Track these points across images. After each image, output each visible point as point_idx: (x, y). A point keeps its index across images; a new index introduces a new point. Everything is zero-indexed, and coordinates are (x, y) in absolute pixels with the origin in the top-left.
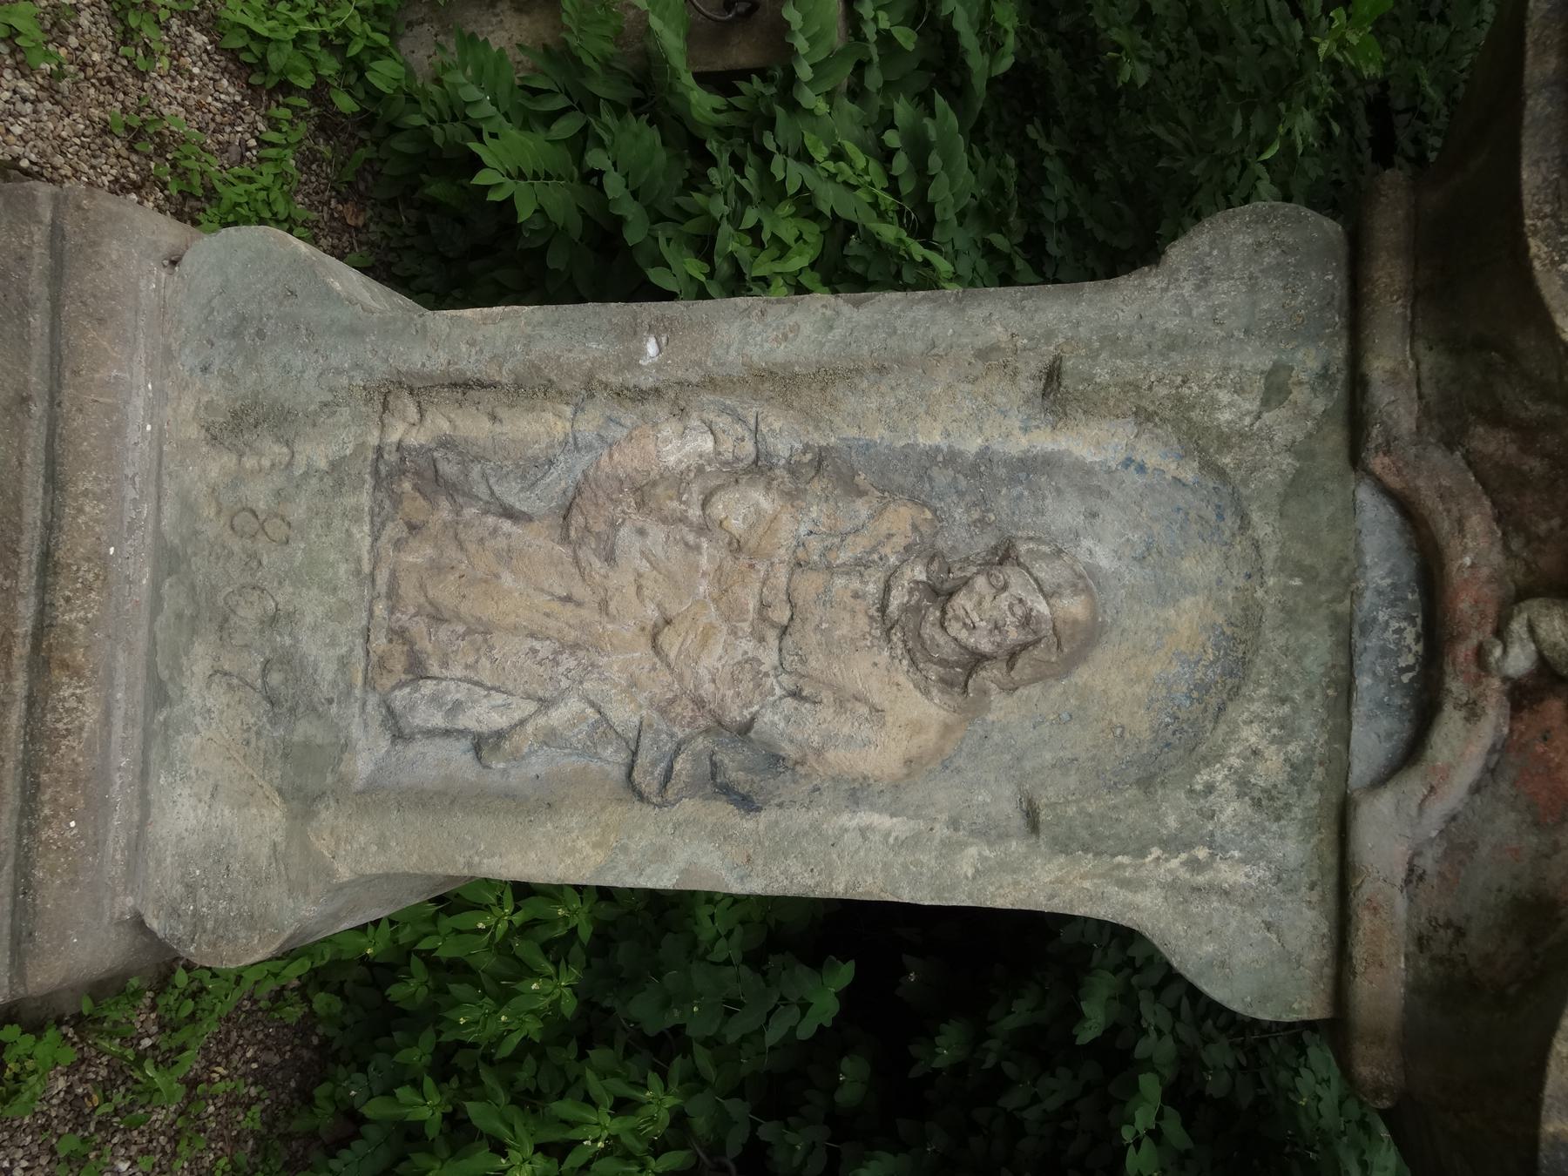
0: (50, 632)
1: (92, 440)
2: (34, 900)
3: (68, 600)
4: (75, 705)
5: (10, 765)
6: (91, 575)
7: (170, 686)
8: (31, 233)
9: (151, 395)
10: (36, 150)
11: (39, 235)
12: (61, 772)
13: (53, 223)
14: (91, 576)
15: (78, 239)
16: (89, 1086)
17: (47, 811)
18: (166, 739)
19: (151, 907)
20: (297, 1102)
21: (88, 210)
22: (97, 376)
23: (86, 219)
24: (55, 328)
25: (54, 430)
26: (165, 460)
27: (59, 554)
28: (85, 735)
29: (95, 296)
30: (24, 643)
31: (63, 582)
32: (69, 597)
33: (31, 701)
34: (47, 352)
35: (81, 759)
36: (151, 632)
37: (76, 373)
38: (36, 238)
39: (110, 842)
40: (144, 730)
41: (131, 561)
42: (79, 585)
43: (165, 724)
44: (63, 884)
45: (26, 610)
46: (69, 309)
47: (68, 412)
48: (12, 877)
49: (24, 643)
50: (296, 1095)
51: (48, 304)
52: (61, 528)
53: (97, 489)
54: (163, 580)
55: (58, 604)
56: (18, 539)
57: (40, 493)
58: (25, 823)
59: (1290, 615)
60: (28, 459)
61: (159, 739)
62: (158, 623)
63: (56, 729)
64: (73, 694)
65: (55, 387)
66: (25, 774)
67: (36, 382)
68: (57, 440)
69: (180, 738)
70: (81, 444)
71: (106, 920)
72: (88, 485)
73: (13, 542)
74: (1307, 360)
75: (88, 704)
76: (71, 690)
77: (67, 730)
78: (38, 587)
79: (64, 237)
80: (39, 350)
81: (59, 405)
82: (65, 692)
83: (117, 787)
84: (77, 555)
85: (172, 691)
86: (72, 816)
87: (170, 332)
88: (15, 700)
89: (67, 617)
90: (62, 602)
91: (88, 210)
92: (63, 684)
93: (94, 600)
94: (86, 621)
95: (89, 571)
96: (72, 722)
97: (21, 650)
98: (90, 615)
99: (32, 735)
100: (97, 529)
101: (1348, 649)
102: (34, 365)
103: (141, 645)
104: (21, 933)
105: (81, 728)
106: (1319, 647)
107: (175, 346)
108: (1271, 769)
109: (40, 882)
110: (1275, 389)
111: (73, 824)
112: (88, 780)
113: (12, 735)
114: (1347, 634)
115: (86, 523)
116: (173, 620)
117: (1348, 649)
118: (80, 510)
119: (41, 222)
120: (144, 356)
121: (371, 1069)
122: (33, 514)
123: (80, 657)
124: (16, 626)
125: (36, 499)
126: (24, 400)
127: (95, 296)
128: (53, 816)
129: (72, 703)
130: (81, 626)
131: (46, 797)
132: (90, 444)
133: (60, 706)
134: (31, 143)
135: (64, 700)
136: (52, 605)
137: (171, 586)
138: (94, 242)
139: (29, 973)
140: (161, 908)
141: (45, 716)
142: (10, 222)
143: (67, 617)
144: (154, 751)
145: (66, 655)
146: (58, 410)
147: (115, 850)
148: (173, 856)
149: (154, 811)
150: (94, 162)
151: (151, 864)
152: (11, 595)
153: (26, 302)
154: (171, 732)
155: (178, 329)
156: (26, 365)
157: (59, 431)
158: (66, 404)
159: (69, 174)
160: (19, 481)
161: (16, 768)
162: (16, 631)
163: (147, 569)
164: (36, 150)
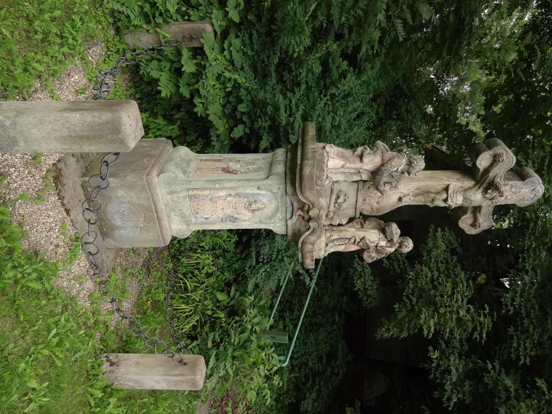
45: (156, 216)
59: (282, 206)
67: (150, 196)
74: (282, 187)
80: (149, 192)
106: (284, 209)
108: (281, 217)
110: (279, 189)
114: (286, 208)
122: (153, 207)
152: (154, 215)
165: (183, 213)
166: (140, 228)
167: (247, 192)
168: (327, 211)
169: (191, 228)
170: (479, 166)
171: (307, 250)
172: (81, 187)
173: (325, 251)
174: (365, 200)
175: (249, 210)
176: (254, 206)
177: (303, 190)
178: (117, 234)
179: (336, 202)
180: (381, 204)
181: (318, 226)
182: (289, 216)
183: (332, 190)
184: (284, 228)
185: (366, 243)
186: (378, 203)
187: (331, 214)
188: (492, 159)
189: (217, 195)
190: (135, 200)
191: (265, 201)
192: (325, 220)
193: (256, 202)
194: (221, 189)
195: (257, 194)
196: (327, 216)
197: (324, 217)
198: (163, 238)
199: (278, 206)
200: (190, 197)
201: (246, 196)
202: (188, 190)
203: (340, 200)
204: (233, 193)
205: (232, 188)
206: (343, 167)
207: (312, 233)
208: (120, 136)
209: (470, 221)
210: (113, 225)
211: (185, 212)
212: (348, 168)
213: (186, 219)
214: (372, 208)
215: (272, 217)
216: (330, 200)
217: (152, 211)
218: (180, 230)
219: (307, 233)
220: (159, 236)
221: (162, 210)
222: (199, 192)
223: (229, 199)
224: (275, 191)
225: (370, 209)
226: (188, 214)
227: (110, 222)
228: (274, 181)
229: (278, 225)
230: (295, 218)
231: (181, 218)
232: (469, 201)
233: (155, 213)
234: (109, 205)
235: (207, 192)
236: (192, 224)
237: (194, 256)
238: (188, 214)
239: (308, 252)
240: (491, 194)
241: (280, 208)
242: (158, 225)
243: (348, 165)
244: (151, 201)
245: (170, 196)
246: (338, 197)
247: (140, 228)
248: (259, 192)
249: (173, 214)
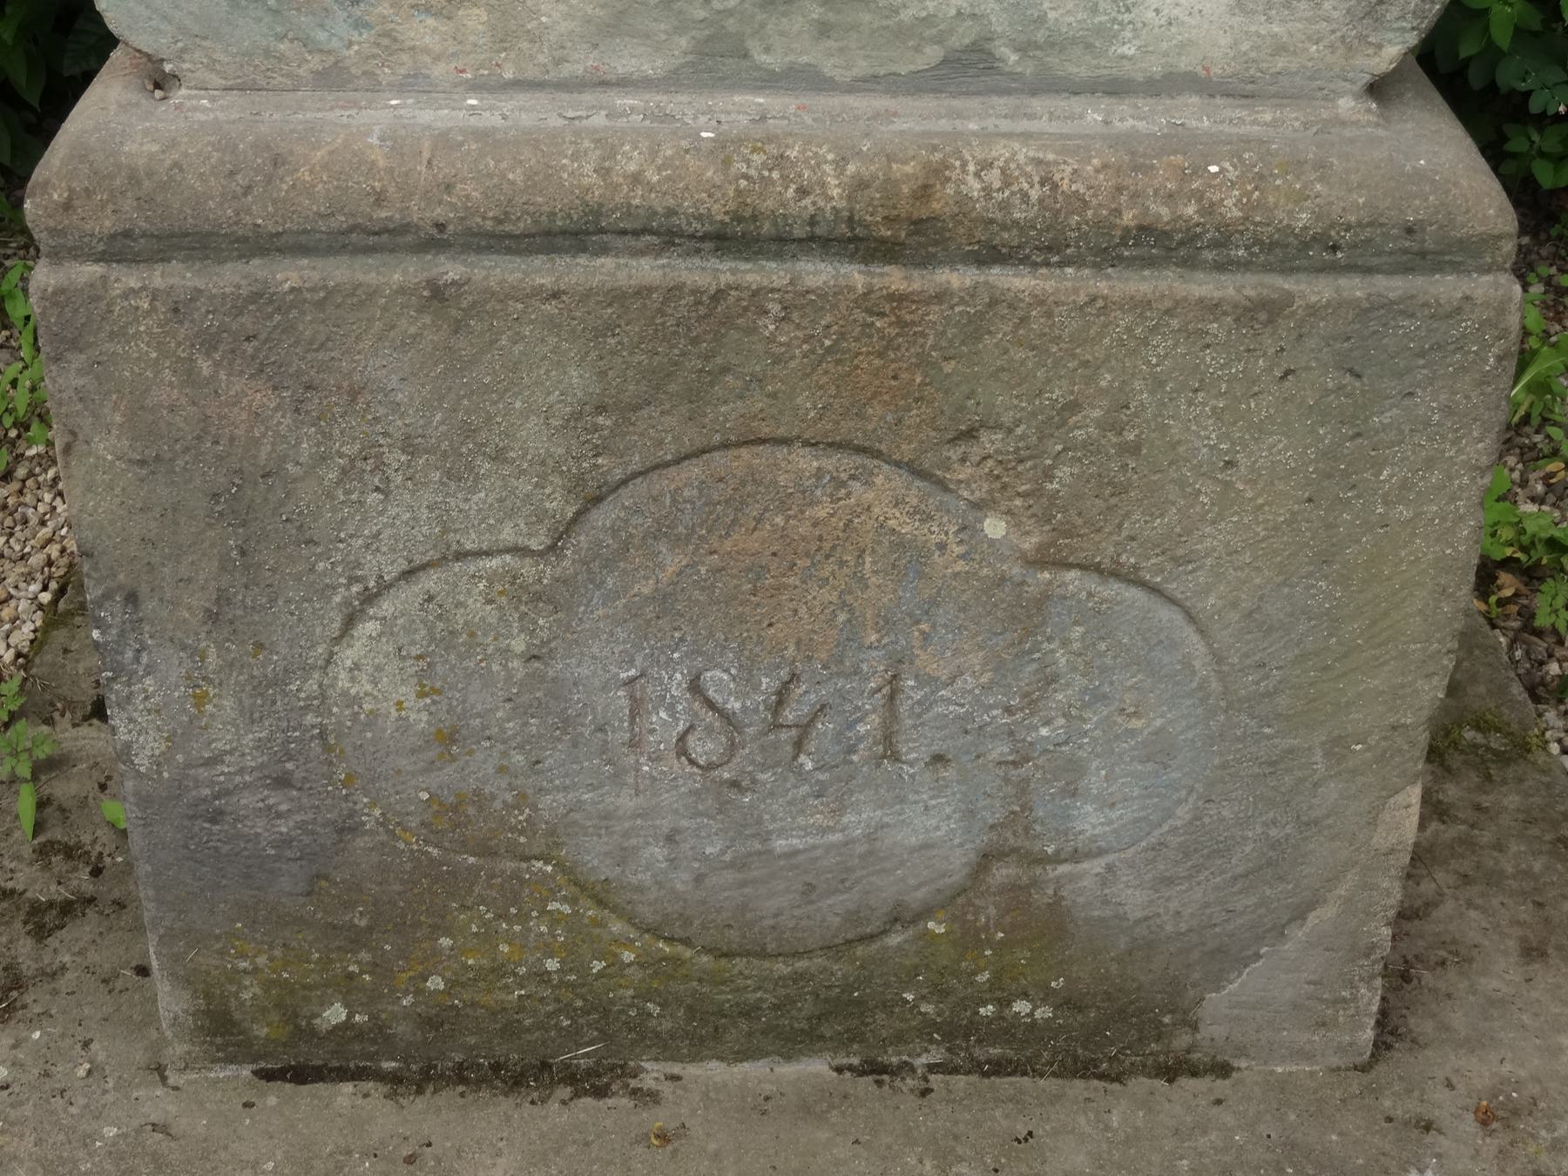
0: (861, 223)
1: (504, 165)
2: (1348, 228)
3: (803, 192)
4: (996, 172)
5: (1103, 286)
6: (755, 157)
7: (955, 42)
8: (129, 293)
9: (410, 101)
10: (22, 585)
11: (129, 278)
12: (1119, 189)
13: (100, 258)
14: (758, 159)
15: (128, 204)
16: (1532, 476)
17: (1190, 210)
18: (1052, 45)
19: (1359, 61)
20: (1554, 232)
21: (71, 190)
22: (382, 163)
23: (88, 192)
24: (300, 245)
25: (491, 235)
26: (531, 73)
27: (719, 212)
28: (1051, 157)
29: (232, 174)
30: (882, 275)
31: (770, 203)
32: (797, 191)
33: (991, 255)
34: (345, 259)
35: (1095, 161)
36: (851, 88)
37: (380, 199)
38: (133, 283)
39: (1243, 130)
40: (1034, 93)
41: (723, 118)
42: (775, 175)
43: (1023, 49)
44: (1321, 179)
45: (817, 273)
46: (260, 216)
47: (453, 207)
48: (1302, 276)
49: (882, 275)
50: (1543, 236)
51: (256, 262)
52: (671, 212)
53: (595, 156)
54: (758, 68)
55: (811, 210)
56: (694, 292)
57: (607, 262)
58: (1209, 255)
60: (546, 281)
61: (1053, 60)
62: (837, 74)
63: (1041, 201)
64: (977, 175)
65: (409, 238)
66: (1121, 258)
67: (404, 272)
68: (508, 228)
69: (1052, 15)
70: (513, 183)
71: (1381, 132)
72: (588, 169)
73: (698, 303)
75: (994, 154)
76: (970, 179)
77: (1042, 184)
78: (779, 256)
79: (127, 234)
80: (340, 271)
81: (441, 227)
82: (974, 187)
83: (1141, 125)
84: (718, 180)
85: (964, 36)
86: (1199, 170)
87: (288, 75)
88: (986, 283)
89: (835, 192)
90: (807, 201)
91: (71, 190)
92: (958, 193)
93: (803, 152)
94: (840, 163)
95: (748, 162)
96: (1028, 176)
97: (894, 278)
98: (830, 157)
99: (1049, 249)
100: (669, 153)
102: (372, 278)
103: (880, 102)
104: (1405, 251)
105: (1039, 162)
107: (315, 62)
109: (1318, 217)
111: (1214, 169)
112: (1133, 154)
113: (1050, 285)
115: (659, 170)
116: (830, 43)
118: (636, 179)
119: (104, 278)
120: (338, 112)
121: (1523, 86)
122: (647, 270)
123: (908, 169)
124: (851, 289)
125: (618, 266)
126: (438, 293)
127: (232, 174)
128: (1200, 200)
129: (994, 177)
130: (851, 168)
131: (1165, 212)
132: (512, 169)
133: (999, 196)
134: (11, 590)
135: (987, 191)
136: (813, 221)
137: (767, 50)
138: (130, 178)
139: (1480, 229)
140: (1362, 38)
141: (1016, 223)
142: (112, 336)
143: (835, 192)
144: (1073, 69)
145: (905, 189)
146: (451, 227)
147: (1255, 122)
148: (1269, 20)
149: (1183, 64)
150: (34, 521)
151: (1280, 63)
152: (797, 303)
153: (255, 297)
154: (1040, 36)
155: (281, 58)
156: (373, 293)
157: (489, 225)
158: (439, 213)
159: (58, 547)
160: (587, 295)
161: (1109, 277)
162: (860, 289)
163: (737, 98)
164: (22, 585)
166: (1039, 560)
172: (273, 1096)
178: (1133, 899)
210: (954, 901)
220: (1269, 310)
221: (723, 150)
227: (898, 918)
233: (769, 273)
234: (594, 857)
237: (1081, 876)
242: (1016, 281)
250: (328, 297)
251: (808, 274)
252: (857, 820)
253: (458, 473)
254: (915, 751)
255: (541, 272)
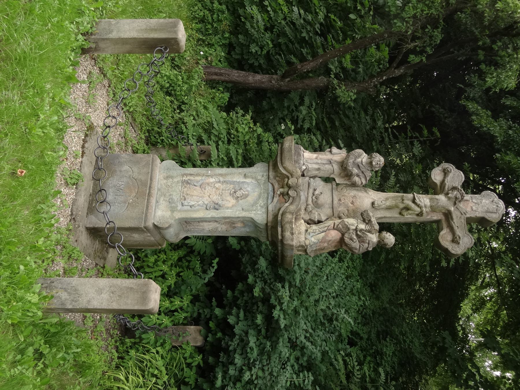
45: (148, 191)
59: (264, 193)
67: (150, 171)
74: (265, 174)
101: (268, 195)
106: (266, 195)
108: (262, 204)
110: (263, 176)
114: (268, 194)
117: (268, 195)
152: (146, 190)
165: (171, 199)
166: (129, 203)
167: (235, 180)
168: (305, 204)
169: (175, 215)
170: (435, 181)
171: (286, 220)
173: (306, 239)
174: (340, 200)
175: (233, 197)
176: (239, 194)
177: (283, 161)
179: (313, 195)
180: (355, 204)
181: (297, 194)
182: (269, 201)
183: (309, 184)
184: (265, 216)
185: (345, 224)
186: (352, 203)
187: (310, 208)
188: (443, 173)
189: (207, 181)
190: (136, 175)
191: (249, 189)
192: (304, 214)
193: (241, 189)
194: (212, 176)
195: (243, 182)
196: (305, 209)
197: (303, 211)
198: (146, 215)
199: (261, 193)
200: (183, 182)
201: (233, 183)
202: (183, 175)
203: (317, 192)
204: (222, 179)
205: (221, 175)
206: (316, 158)
207: (291, 204)
208: (175, 29)
209: (450, 237)
211: (174, 197)
212: (321, 159)
213: (173, 205)
214: (348, 210)
215: (255, 203)
216: (308, 194)
217: (146, 186)
218: (163, 217)
219: (287, 204)
220: (143, 213)
222: (192, 178)
223: (217, 185)
224: (259, 178)
225: (347, 212)
226: (176, 200)
228: (259, 169)
229: (259, 212)
230: (275, 200)
231: (168, 203)
232: (435, 200)
233: (148, 189)
234: (111, 179)
235: (198, 178)
236: (177, 210)
238: (176, 200)
239: (288, 222)
240: (452, 193)
241: (263, 195)
243: (320, 156)
244: (150, 176)
245: (165, 181)
246: (315, 190)
247: (129, 203)
248: (244, 180)
249: (162, 199)
250: (149, 167)
251: (228, 300)
252: (111, 194)
253: (138, 173)
254: (116, 197)
255: (149, 178)
